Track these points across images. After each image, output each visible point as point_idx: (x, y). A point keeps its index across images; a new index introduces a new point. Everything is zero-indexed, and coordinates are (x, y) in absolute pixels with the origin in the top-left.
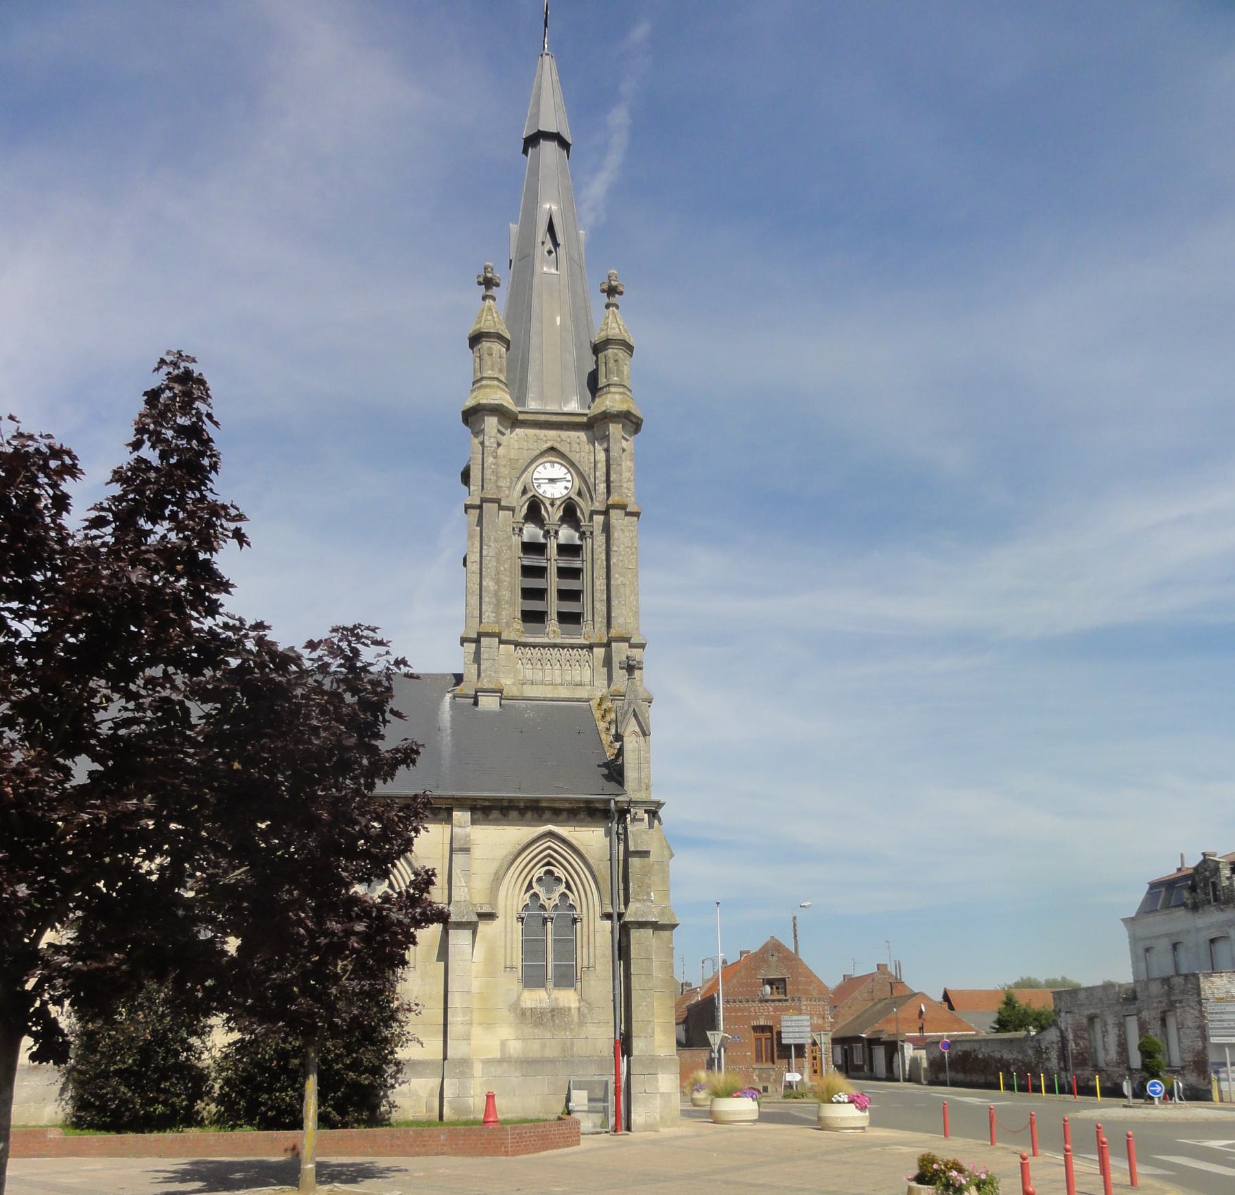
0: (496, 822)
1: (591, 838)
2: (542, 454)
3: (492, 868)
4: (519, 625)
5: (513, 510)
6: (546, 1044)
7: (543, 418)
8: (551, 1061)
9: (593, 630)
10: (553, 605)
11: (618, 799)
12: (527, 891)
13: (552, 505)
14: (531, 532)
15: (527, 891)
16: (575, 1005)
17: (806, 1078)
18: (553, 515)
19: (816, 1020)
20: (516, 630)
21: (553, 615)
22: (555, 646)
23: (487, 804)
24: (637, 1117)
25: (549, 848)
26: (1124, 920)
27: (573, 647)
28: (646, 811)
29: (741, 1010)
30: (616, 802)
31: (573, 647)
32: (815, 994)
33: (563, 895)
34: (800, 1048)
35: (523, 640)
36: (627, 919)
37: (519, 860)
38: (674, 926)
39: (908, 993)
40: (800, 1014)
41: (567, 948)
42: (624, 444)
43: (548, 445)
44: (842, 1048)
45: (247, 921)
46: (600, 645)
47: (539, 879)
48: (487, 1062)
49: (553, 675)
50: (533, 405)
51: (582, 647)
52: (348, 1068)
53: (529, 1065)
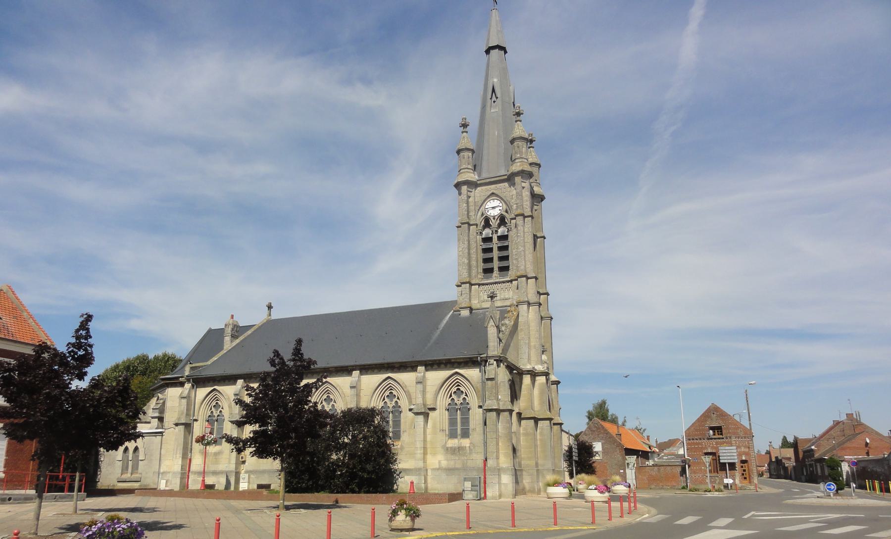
0: (436, 370)
1: (473, 373)
2: (489, 197)
3: (435, 388)
4: (481, 276)
5: (477, 225)
6: (456, 462)
7: (488, 180)
9: (512, 274)
10: (496, 264)
14: (487, 232)
16: (468, 445)
17: (737, 482)
18: (494, 223)
20: (478, 277)
22: (496, 283)
24: (489, 494)
26: (604, 403)
27: (504, 282)
31: (504, 282)
32: (741, 434)
33: (464, 399)
34: (732, 466)
41: (466, 421)
42: (524, 185)
48: (433, 469)
50: (484, 175)
51: (508, 282)
52: (359, 471)
53: (450, 471)
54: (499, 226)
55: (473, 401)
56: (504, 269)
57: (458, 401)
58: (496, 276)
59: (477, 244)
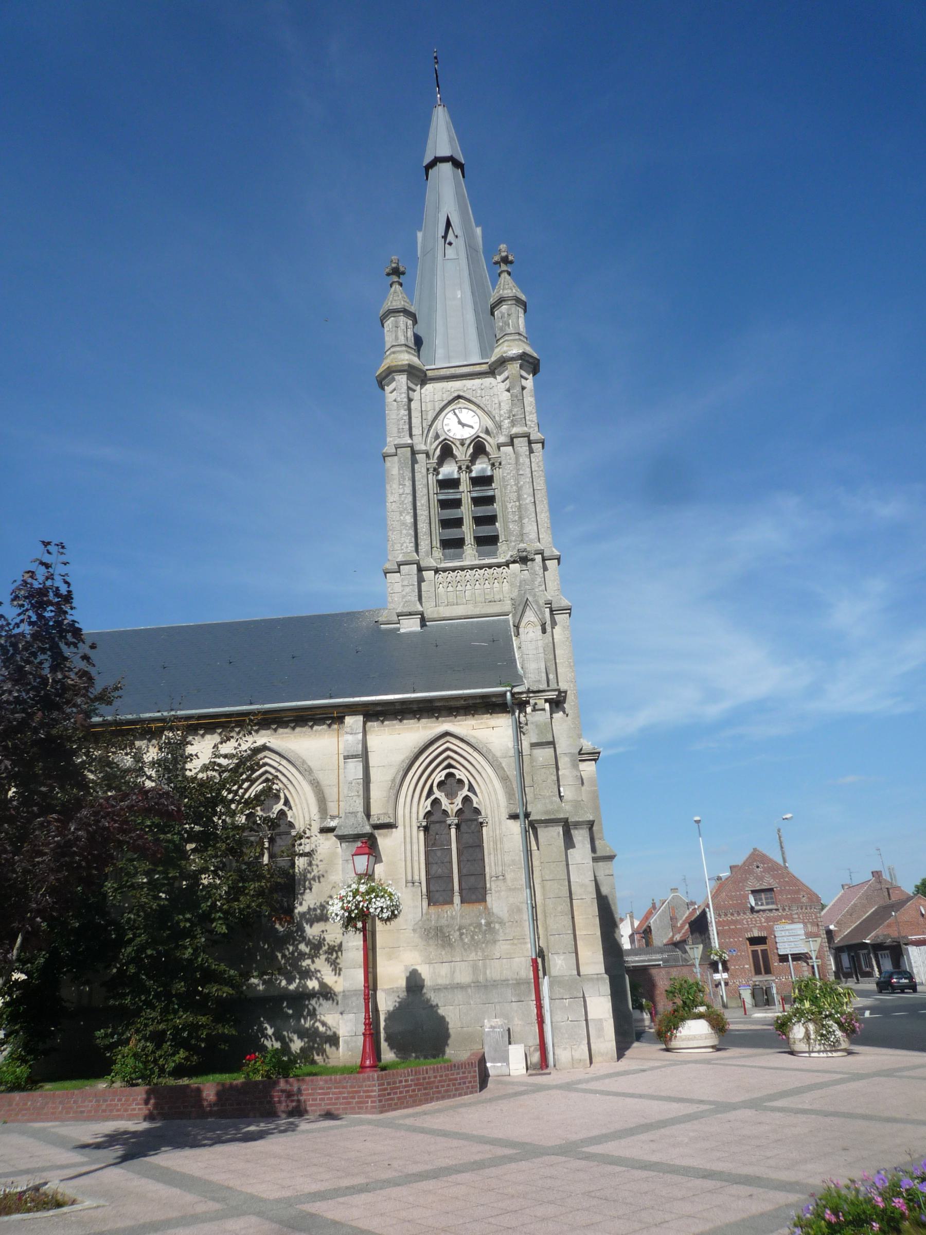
1: (495, 731)
2: (450, 403)
4: (438, 553)
9: (504, 552)
10: (468, 530)
11: (516, 690)
12: (428, 797)
13: (463, 445)
14: (449, 470)
15: (428, 797)
20: (434, 558)
21: (469, 539)
23: (379, 708)
25: (448, 749)
28: (546, 701)
29: (735, 922)
30: (513, 695)
31: (490, 566)
32: (804, 900)
35: (443, 565)
39: (904, 897)
40: (793, 922)
41: (473, 848)
43: (456, 394)
44: (849, 955)
45: (88, 854)
47: (441, 784)
49: (466, 594)
54: (474, 458)
55: (492, 798)
56: (487, 542)
57: (451, 806)
58: (470, 555)
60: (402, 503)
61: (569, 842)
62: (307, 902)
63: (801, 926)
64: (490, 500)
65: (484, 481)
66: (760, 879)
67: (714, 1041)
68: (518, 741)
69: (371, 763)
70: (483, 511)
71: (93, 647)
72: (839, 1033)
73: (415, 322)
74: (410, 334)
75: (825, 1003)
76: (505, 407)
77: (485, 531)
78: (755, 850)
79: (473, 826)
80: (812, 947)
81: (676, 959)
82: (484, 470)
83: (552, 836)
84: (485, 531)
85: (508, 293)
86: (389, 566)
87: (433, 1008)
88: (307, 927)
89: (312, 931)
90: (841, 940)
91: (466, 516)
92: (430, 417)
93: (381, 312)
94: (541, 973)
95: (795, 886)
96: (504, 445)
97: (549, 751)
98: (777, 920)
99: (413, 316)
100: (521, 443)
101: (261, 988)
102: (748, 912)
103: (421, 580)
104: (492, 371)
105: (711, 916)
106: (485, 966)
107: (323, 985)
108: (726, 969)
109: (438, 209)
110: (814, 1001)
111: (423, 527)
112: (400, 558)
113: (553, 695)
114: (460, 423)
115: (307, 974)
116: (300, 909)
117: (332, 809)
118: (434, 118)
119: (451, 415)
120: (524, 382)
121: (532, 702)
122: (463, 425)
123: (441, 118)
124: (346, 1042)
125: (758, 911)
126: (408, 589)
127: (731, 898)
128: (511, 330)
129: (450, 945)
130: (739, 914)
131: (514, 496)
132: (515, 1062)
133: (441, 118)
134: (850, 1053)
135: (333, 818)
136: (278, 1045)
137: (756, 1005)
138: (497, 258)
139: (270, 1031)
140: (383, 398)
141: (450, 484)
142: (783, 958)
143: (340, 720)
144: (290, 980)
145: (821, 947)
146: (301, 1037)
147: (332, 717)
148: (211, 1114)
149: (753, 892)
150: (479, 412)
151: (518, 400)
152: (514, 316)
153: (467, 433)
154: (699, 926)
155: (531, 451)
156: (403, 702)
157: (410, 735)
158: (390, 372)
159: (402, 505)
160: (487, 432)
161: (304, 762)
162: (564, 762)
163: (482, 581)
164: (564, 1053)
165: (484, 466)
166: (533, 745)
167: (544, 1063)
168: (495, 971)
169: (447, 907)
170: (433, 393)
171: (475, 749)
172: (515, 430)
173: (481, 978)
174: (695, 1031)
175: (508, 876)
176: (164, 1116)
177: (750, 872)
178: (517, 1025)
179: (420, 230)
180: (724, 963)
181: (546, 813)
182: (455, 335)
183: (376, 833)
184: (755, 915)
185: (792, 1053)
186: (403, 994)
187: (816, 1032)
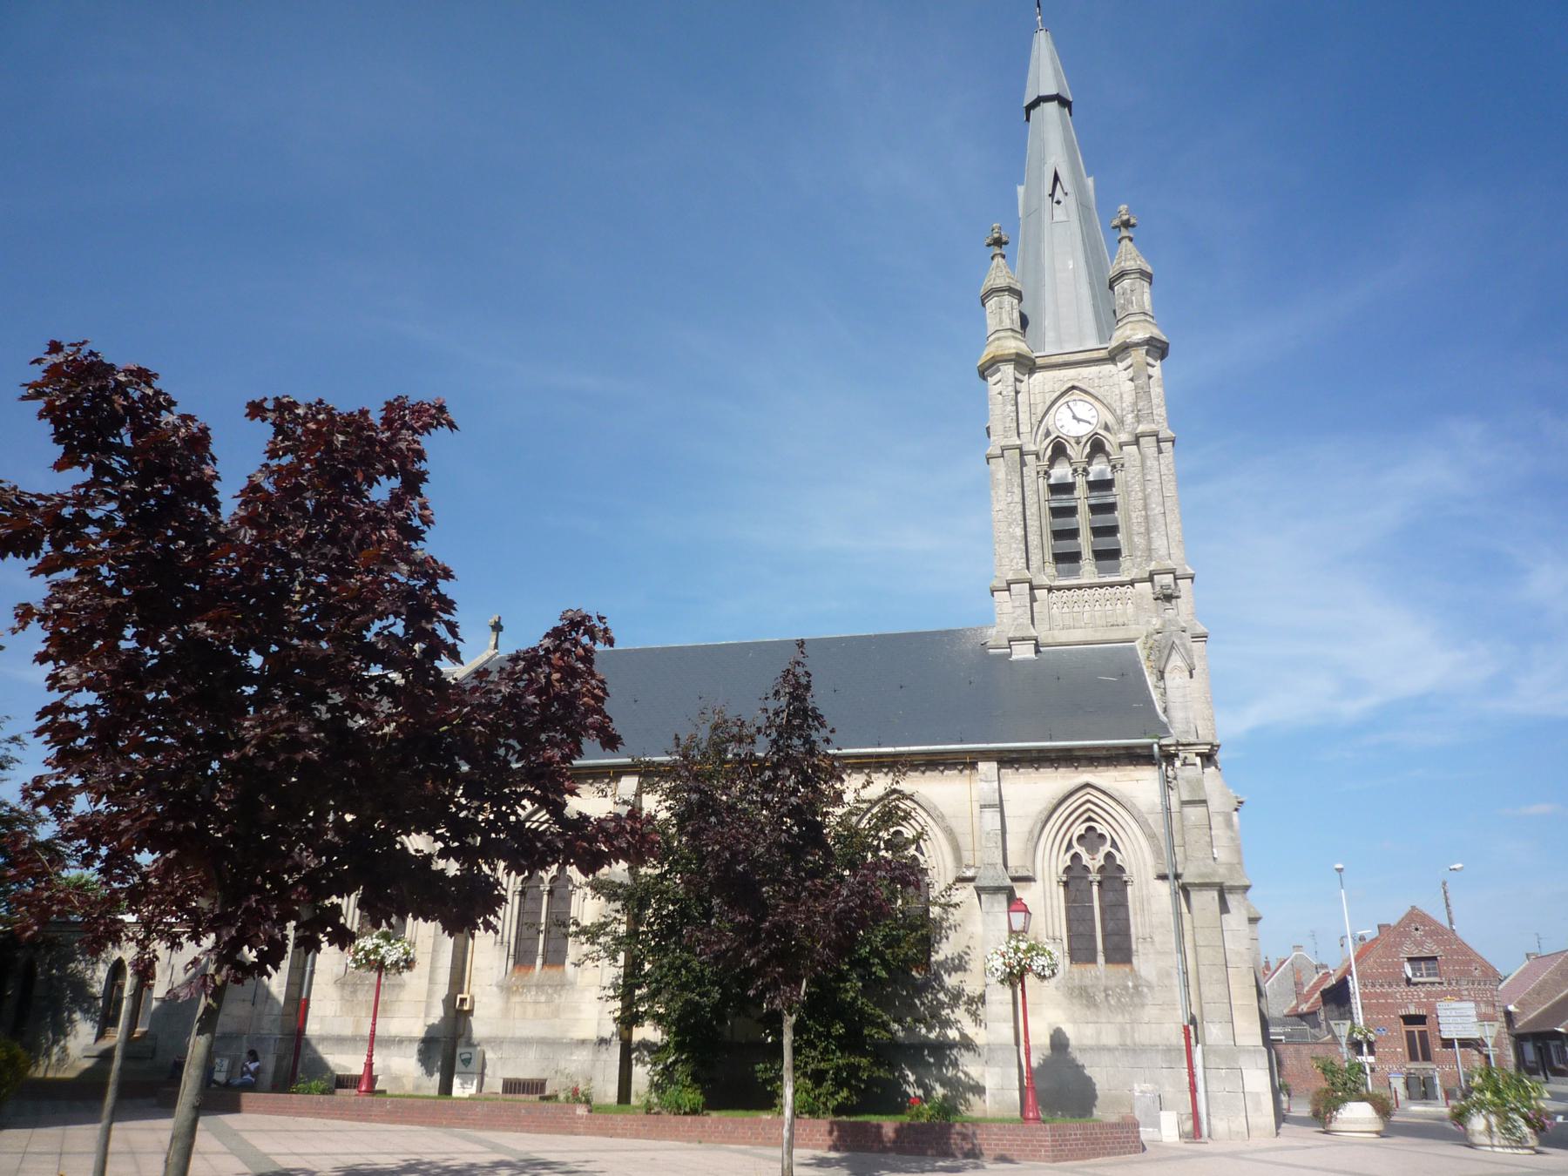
1: (1140, 785)
4: (1051, 569)
8: (1109, 1049)
9: (1129, 568)
10: (1085, 542)
11: (1164, 742)
12: (1068, 849)
13: (1078, 443)
14: (1061, 472)
18: (1077, 453)
19: (1483, 1009)
20: (1047, 574)
21: (1087, 553)
29: (1385, 996)
30: (1160, 747)
32: (1477, 973)
35: (1057, 583)
36: (1186, 879)
37: (1056, 816)
38: (1246, 888)
41: (1117, 907)
46: (1142, 581)
47: (1081, 838)
49: (1085, 617)
54: (1090, 457)
55: (1138, 858)
56: (1107, 556)
58: (1088, 570)
59: (1039, 500)
60: (1011, 513)
61: (1224, 908)
62: (944, 951)
63: (1472, 1005)
64: (1111, 508)
65: (1104, 485)
66: (1420, 944)
67: (1379, 1126)
68: (1166, 797)
69: (1006, 813)
70: (1103, 520)
71: (832, 731)
72: (1526, 1129)
73: (1020, 300)
74: (1016, 315)
75: (1510, 1095)
76: (1129, 399)
77: (1105, 543)
78: (1413, 908)
79: (1117, 885)
80: (1490, 1033)
81: (1303, 1035)
82: (1102, 472)
83: (1205, 901)
84: (1105, 543)
85: (1130, 265)
86: (996, 583)
87: (1079, 1069)
88: (945, 977)
89: (951, 981)
90: (1526, 1024)
91: (1082, 528)
92: (1040, 410)
93: (982, 292)
94: (1193, 1041)
95: (1465, 957)
96: (1127, 444)
97: (1200, 810)
98: (1442, 995)
99: (1018, 294)
100: (1148, 444)
101: (901, 1034)
102: (1403, 984)
103: (1033, 599)
104: (1112, 357)
105: (1354, 985)
106: (1133, 1029)
107: (963, 1036)
108: (1372, 1052)
109: (1042, 161)
110: (1497, 1092)
111: (1034, 539)
112: (1010, 576)
113: (1205, 749)
114: (1074, 417)
115: (946, 1023)
116: (935, 958)
117: (967, 857)
118: (1035, 46)
119: (1065, 407)
120: (1150, 370)
121: (1181, 755)
122: (1079, 420)
123: (1043, 44)
124: (993, 1095)
125: (1416, 984)
126: (1019, 611)
127: (1381, 966)
128: (1135, 309)
129: (1095, 1005)
130: (1390, 985)
131: (1140, 504)
132: (1168, 1128)
133: (1043, 44)
134: (1538, 1152)
135: (968, 867)
136: (920, 1092)
137: (1410, 1098)
138: (1116, 222)
139: (912, 1078)
140: (986, 390)
141: (1067, 488)
142: (1448, 1043)
143: (973, 765)
144: (930, 1029)
145: (1499, 1033)
146: (943, 1085)
147: (966, 762)
148: (890, 1150)
149: (1410, 960)
150: (1097, 404)
151: (1142, 392)
152: (1138, 292)
153: (1083, 430)
154: (1337, 996)
155: (1160, 451)
156: (1040, 750)
157: (1051, 783)
158: (994, 363)
159: (1009, 518)
160: (1107, 428)
161: (936, 808)
162: (1217, 821)
163: (1103, 602)
164: (1219, 1124)
165: (1103, 467)
166: (1184, 803)
167: (1196, 1133)
168: (1144, 1035)
169: (1090, 966)
170: (1042, 384)
171: (1119, 803)
172: (1141, 428)
173: (1128, 1042)
174: (1357, 1115)
175: (1156, 939)
176: (847, 1149)
177: (1407, 935)
178: (1168, 1091)
179: (1021, 184)
180: (1370, 1045)
181: (1201, 876)
182: (1068, 318)
183: (1015, 885)
184: (1412, 988)
185: (1472, 1146)
186: (1048, 1052)
187: (1499, 1125)
